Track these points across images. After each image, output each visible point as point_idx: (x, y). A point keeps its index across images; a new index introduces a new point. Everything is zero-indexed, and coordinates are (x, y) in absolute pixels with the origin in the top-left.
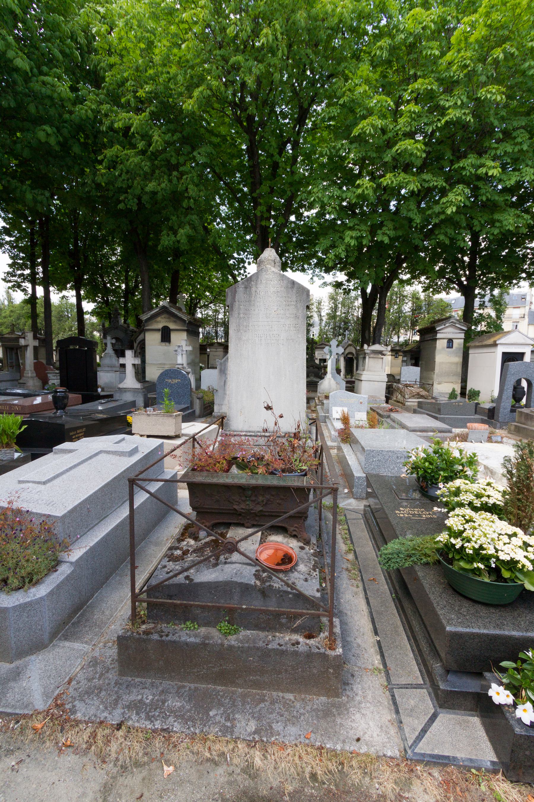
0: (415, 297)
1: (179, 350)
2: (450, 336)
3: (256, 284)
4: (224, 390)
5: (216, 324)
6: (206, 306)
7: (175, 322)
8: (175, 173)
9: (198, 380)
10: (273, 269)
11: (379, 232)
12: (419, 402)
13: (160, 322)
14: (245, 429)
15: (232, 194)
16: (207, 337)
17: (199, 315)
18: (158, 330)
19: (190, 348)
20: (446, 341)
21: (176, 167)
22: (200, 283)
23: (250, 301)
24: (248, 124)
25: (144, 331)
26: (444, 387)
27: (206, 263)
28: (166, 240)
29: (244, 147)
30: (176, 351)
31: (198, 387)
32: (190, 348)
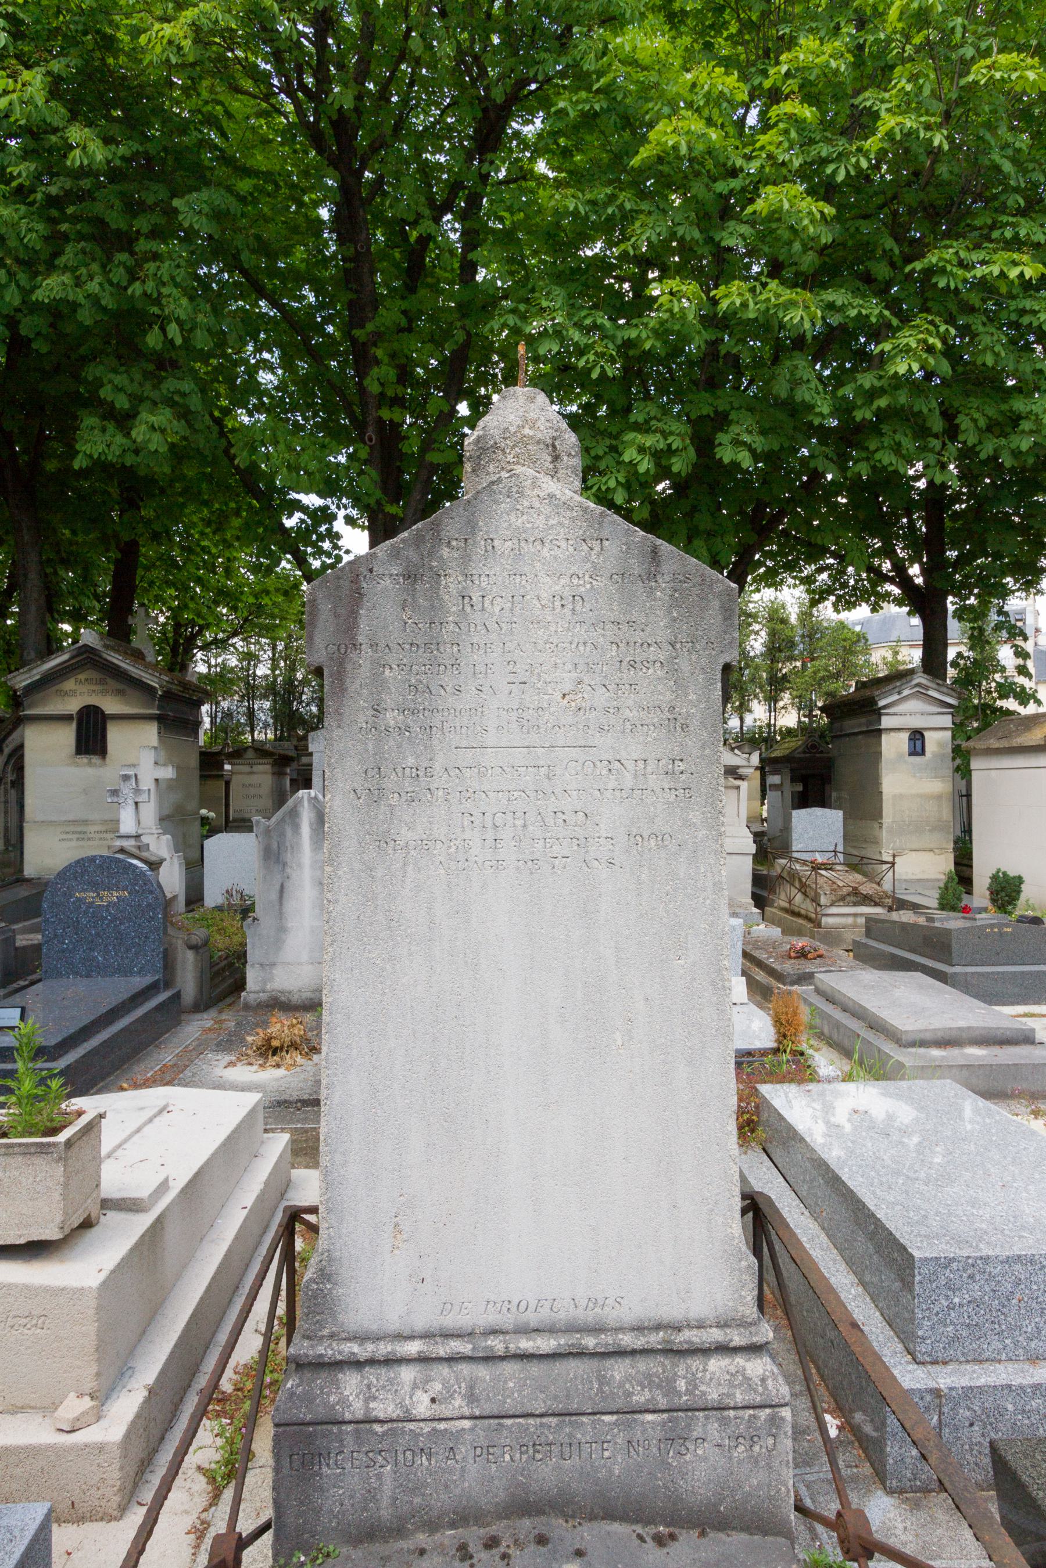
0: (776, 617)
1: (127, 789)
2: (917, 723)
3: (466, 559)
4: (281, 915)
5: (251, 692)
6: (221, 644)
7: (121, 693)
8: (122, 257)
9: (195, 867)
10: (550, 486)
11: (722, 438)
12: (870, 920)
13: (72, 693)
14: (420, 1322)
15: (295, 334)
16: (224, 726)
17: (202, 669)
18: (66, 718)
19: (168, 773)
20: (905, 736)
21: (126, 241)
22: (199, 581)
23: (433, 644)
24: (338, 149)
25: (19, 721)
26: (918, 866)
27: (218, 523)
28: (95, 443)
29: (324, 213)
30: (115, 792)
31: (195, 896)
32: (168, 773)
